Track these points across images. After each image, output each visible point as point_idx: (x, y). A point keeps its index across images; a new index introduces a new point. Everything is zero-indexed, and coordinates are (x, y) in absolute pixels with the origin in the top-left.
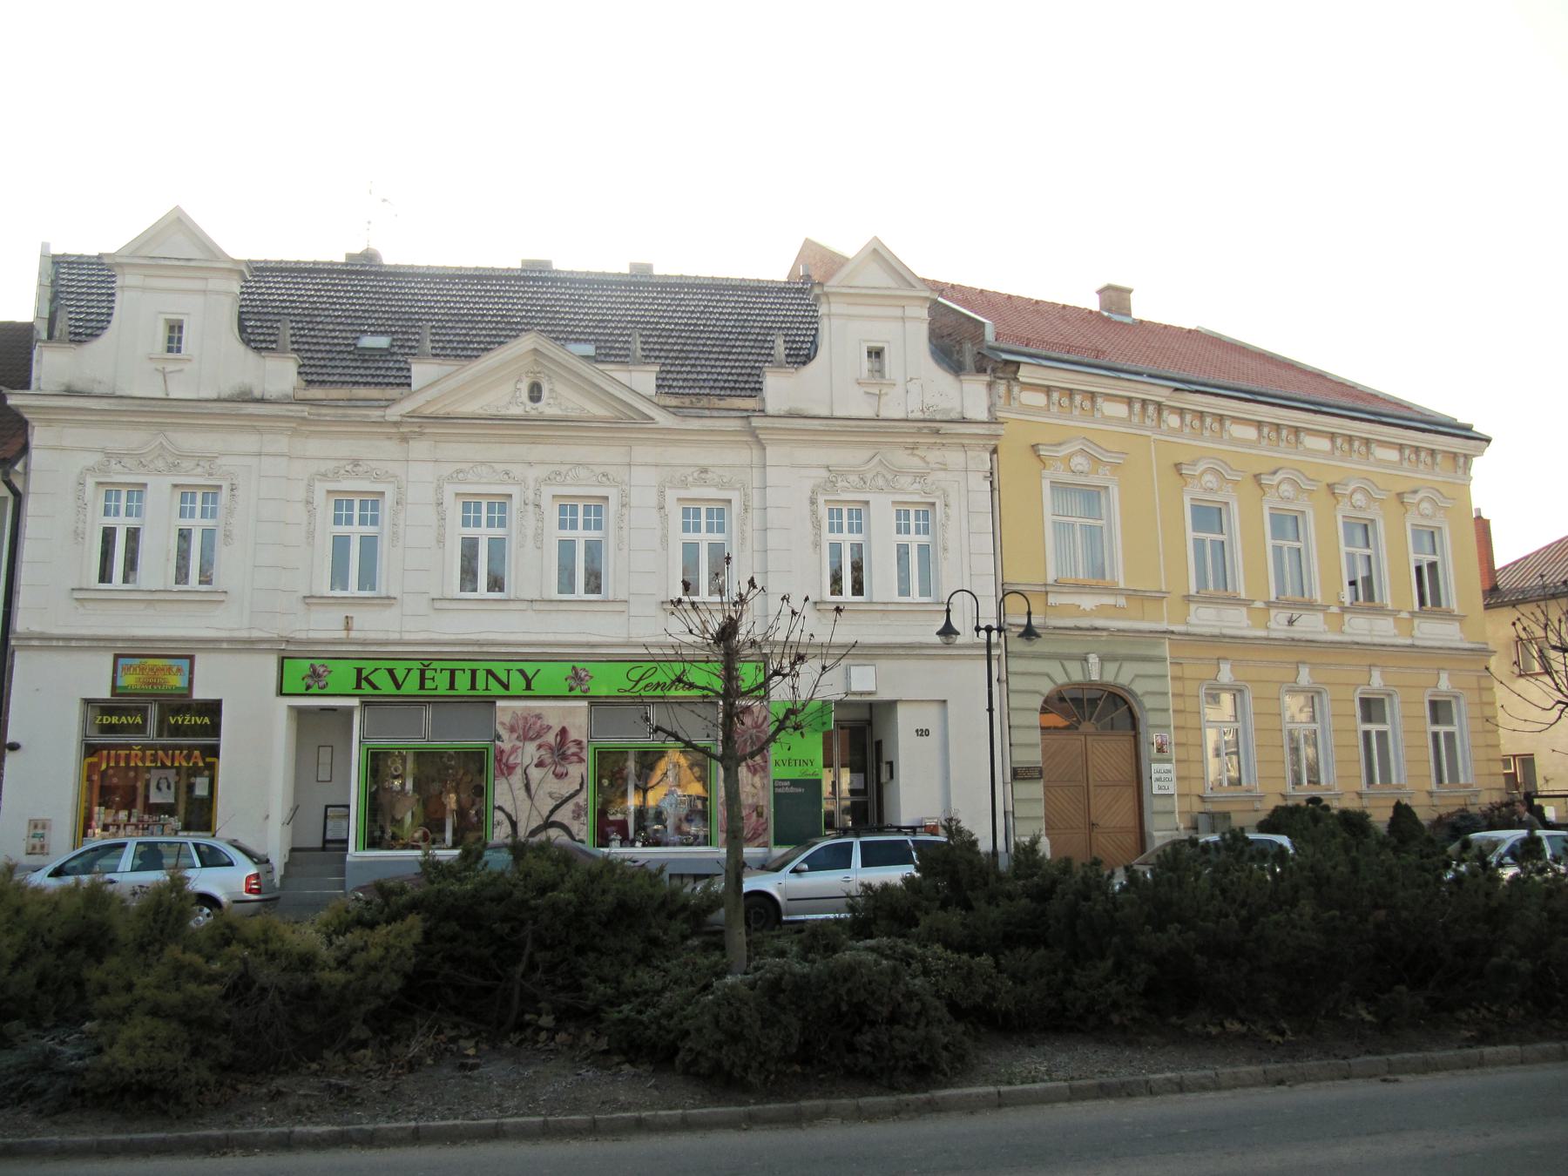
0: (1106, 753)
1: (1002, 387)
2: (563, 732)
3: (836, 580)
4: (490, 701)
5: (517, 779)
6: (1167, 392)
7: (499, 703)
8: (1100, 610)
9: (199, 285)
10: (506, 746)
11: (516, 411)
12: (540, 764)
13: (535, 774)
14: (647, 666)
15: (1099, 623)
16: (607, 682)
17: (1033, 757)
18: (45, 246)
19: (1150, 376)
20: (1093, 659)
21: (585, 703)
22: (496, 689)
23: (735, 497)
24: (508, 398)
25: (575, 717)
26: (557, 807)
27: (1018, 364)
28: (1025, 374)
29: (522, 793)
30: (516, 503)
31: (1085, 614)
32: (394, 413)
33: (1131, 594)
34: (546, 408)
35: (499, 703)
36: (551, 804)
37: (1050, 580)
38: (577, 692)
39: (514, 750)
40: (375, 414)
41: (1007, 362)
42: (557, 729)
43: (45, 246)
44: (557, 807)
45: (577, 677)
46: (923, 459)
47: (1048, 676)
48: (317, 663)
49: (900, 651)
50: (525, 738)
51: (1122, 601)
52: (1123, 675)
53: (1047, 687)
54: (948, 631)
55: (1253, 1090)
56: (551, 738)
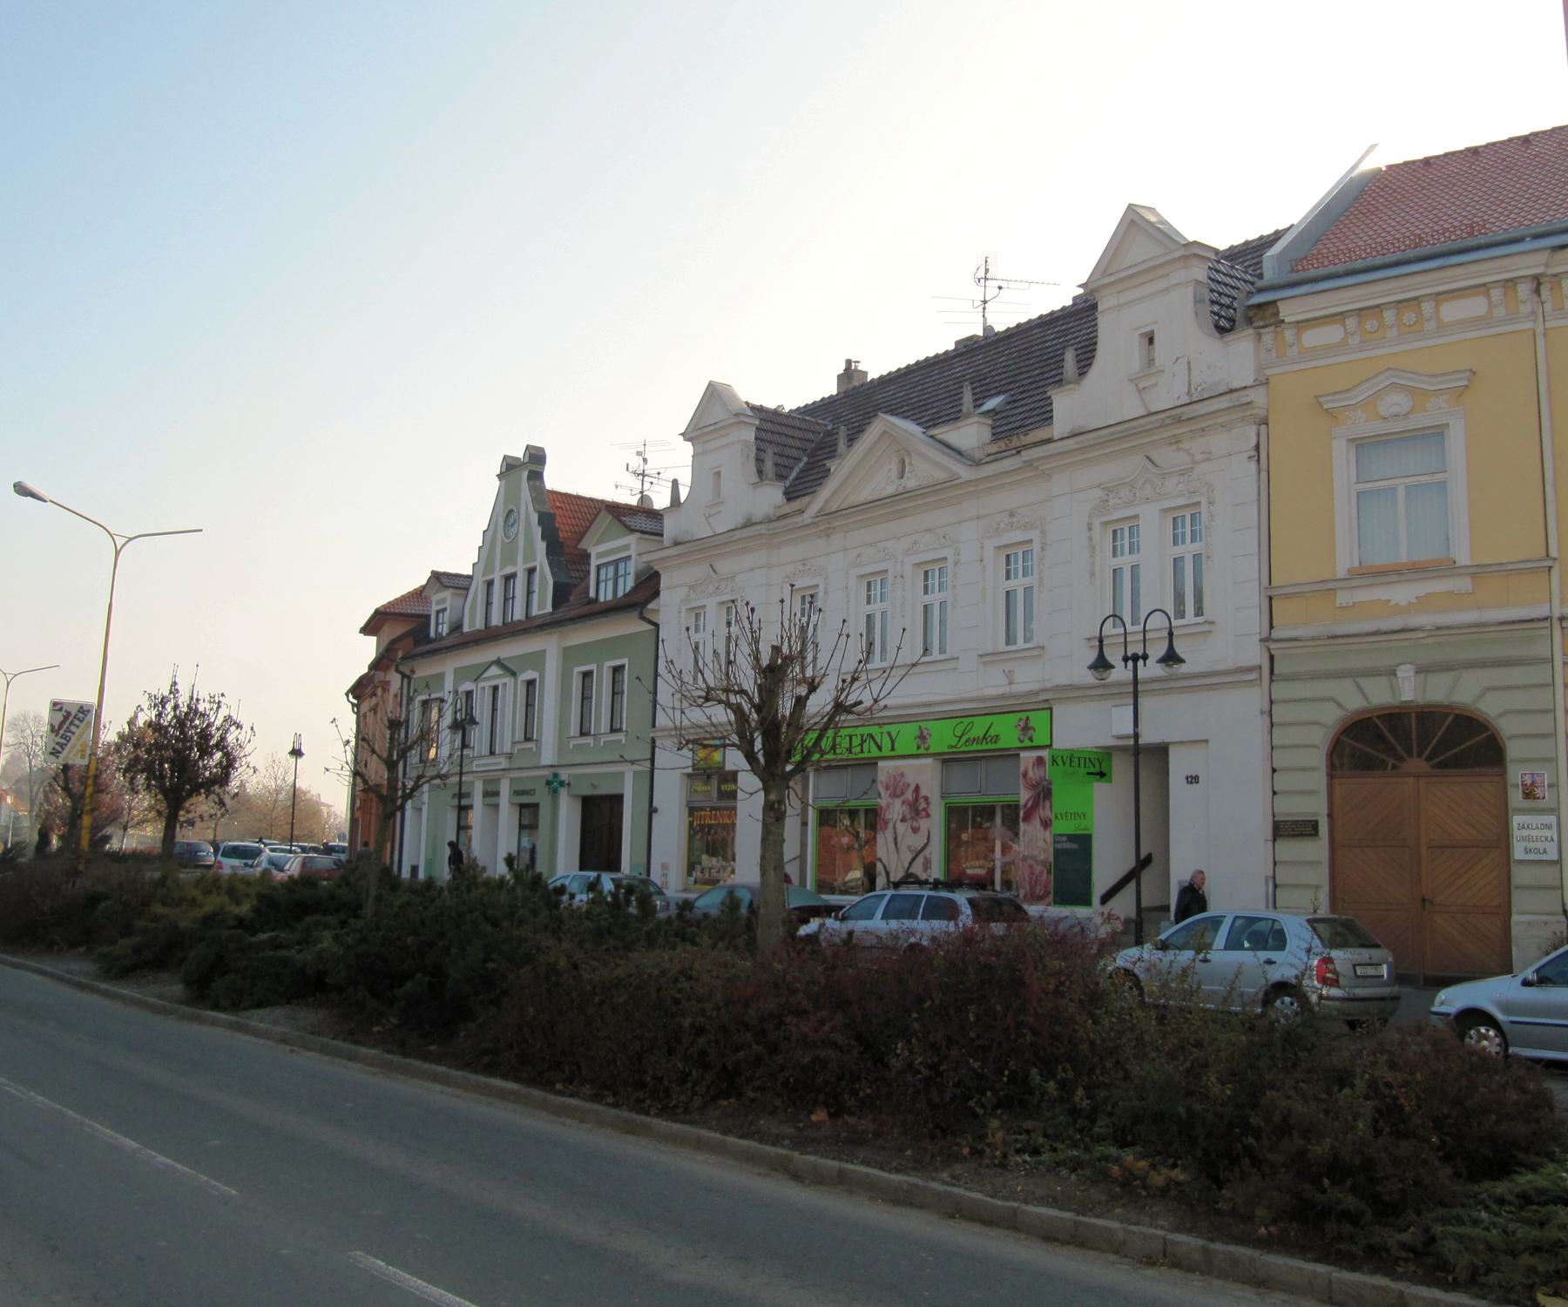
0: (1442, 801)
1: (1268, 338)
2: (917, 789)
3: (1179, 598)
4: (872, 763)
5: (889, 833)
6: (1543, 257)
7: (880, 764)
8: (1423, 602)
9: (722, 442)
10: (883, 802)
11: (890, 490)
12: (903, 820)
13: (901, 828)
14: (967, 720)
15: (1415, 621)
16: (943, 737)
17: (1315, 806)
18: (525, 469)
19: (1536, 237)
20: (1406, 672)
21: (929, 761)
22: (875, 753)
23: (1035, 535)
24: (882, 482)
25: (925, 775)
26: (913, 860)
27: (1273, 303)
28: (1290, 311)
29: (892, 846)
30: (890, 575)
31: (1398, 610)
32: (807, 517)
33: (1478, 572)
34: (911, 483)
35: (880, 764)
36: (910, 856)
37: (1341, 572)
38: (922, 751)
39: (888, 805)
40: (798, 519)
41: (1260, 306)
42: (913, 787)
43: (525, 469)
44: (913, 860)
45: (922, 737)
46: (1187, 451)
47: (1333, 699)
48: (923, 725)
49: (1155, 686)
50: (894, 795)
51: (1463, 584)
52: (1463, 691)
53: (1331, 717)
54: (1101, 664)
55: (1064, 1251)
56: (909, 795)
